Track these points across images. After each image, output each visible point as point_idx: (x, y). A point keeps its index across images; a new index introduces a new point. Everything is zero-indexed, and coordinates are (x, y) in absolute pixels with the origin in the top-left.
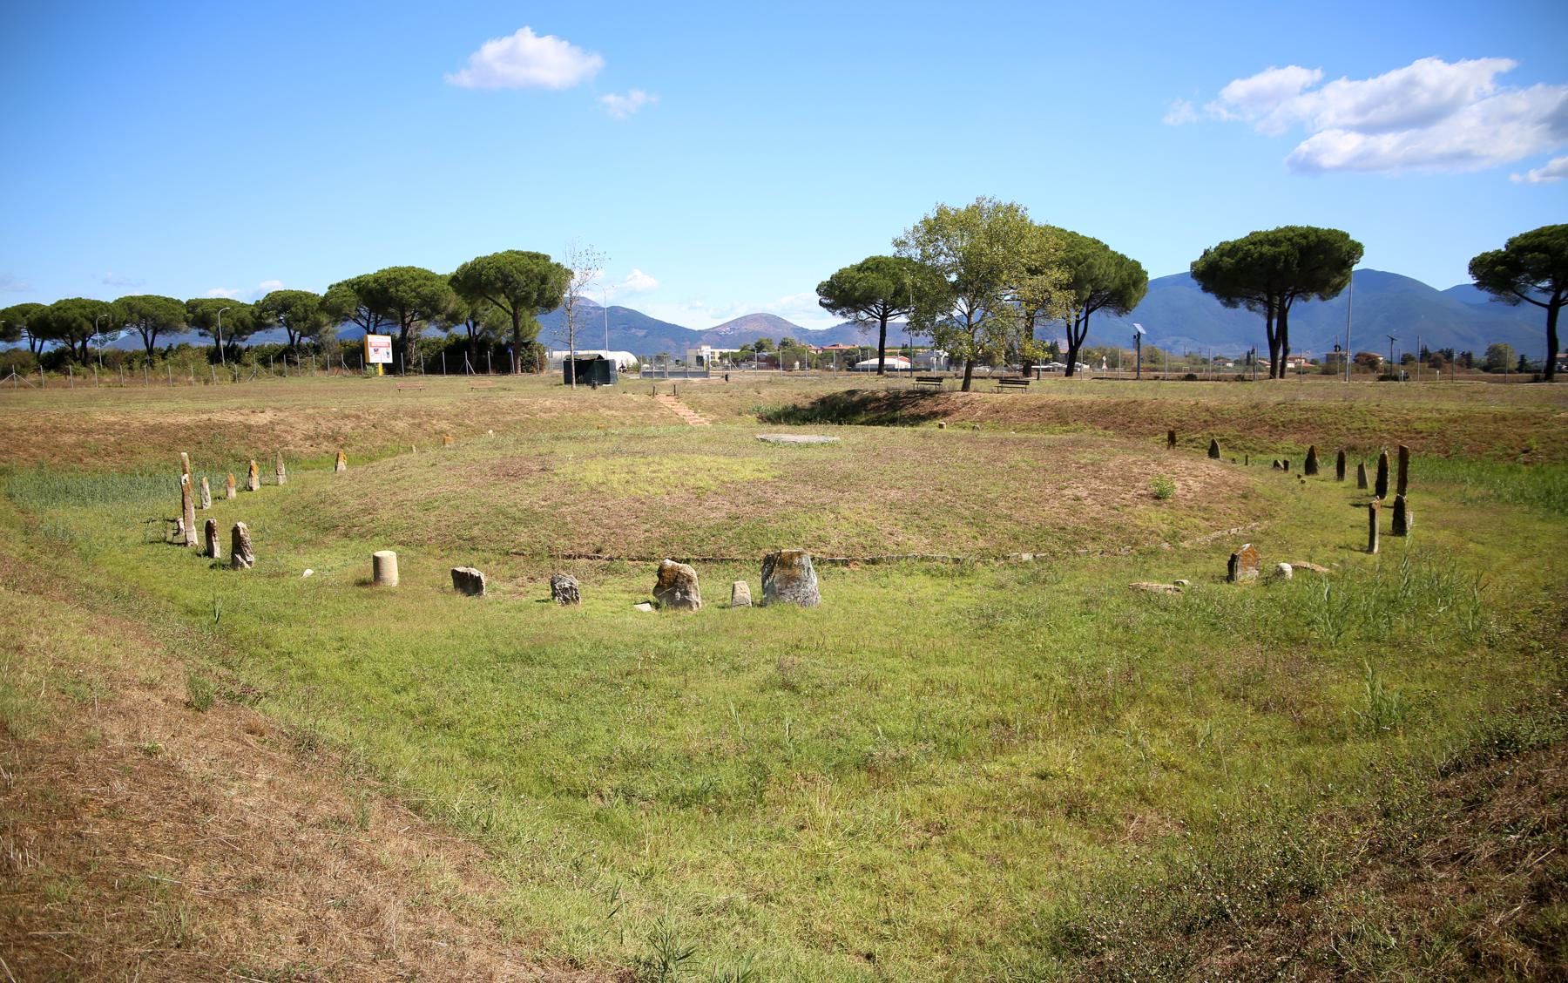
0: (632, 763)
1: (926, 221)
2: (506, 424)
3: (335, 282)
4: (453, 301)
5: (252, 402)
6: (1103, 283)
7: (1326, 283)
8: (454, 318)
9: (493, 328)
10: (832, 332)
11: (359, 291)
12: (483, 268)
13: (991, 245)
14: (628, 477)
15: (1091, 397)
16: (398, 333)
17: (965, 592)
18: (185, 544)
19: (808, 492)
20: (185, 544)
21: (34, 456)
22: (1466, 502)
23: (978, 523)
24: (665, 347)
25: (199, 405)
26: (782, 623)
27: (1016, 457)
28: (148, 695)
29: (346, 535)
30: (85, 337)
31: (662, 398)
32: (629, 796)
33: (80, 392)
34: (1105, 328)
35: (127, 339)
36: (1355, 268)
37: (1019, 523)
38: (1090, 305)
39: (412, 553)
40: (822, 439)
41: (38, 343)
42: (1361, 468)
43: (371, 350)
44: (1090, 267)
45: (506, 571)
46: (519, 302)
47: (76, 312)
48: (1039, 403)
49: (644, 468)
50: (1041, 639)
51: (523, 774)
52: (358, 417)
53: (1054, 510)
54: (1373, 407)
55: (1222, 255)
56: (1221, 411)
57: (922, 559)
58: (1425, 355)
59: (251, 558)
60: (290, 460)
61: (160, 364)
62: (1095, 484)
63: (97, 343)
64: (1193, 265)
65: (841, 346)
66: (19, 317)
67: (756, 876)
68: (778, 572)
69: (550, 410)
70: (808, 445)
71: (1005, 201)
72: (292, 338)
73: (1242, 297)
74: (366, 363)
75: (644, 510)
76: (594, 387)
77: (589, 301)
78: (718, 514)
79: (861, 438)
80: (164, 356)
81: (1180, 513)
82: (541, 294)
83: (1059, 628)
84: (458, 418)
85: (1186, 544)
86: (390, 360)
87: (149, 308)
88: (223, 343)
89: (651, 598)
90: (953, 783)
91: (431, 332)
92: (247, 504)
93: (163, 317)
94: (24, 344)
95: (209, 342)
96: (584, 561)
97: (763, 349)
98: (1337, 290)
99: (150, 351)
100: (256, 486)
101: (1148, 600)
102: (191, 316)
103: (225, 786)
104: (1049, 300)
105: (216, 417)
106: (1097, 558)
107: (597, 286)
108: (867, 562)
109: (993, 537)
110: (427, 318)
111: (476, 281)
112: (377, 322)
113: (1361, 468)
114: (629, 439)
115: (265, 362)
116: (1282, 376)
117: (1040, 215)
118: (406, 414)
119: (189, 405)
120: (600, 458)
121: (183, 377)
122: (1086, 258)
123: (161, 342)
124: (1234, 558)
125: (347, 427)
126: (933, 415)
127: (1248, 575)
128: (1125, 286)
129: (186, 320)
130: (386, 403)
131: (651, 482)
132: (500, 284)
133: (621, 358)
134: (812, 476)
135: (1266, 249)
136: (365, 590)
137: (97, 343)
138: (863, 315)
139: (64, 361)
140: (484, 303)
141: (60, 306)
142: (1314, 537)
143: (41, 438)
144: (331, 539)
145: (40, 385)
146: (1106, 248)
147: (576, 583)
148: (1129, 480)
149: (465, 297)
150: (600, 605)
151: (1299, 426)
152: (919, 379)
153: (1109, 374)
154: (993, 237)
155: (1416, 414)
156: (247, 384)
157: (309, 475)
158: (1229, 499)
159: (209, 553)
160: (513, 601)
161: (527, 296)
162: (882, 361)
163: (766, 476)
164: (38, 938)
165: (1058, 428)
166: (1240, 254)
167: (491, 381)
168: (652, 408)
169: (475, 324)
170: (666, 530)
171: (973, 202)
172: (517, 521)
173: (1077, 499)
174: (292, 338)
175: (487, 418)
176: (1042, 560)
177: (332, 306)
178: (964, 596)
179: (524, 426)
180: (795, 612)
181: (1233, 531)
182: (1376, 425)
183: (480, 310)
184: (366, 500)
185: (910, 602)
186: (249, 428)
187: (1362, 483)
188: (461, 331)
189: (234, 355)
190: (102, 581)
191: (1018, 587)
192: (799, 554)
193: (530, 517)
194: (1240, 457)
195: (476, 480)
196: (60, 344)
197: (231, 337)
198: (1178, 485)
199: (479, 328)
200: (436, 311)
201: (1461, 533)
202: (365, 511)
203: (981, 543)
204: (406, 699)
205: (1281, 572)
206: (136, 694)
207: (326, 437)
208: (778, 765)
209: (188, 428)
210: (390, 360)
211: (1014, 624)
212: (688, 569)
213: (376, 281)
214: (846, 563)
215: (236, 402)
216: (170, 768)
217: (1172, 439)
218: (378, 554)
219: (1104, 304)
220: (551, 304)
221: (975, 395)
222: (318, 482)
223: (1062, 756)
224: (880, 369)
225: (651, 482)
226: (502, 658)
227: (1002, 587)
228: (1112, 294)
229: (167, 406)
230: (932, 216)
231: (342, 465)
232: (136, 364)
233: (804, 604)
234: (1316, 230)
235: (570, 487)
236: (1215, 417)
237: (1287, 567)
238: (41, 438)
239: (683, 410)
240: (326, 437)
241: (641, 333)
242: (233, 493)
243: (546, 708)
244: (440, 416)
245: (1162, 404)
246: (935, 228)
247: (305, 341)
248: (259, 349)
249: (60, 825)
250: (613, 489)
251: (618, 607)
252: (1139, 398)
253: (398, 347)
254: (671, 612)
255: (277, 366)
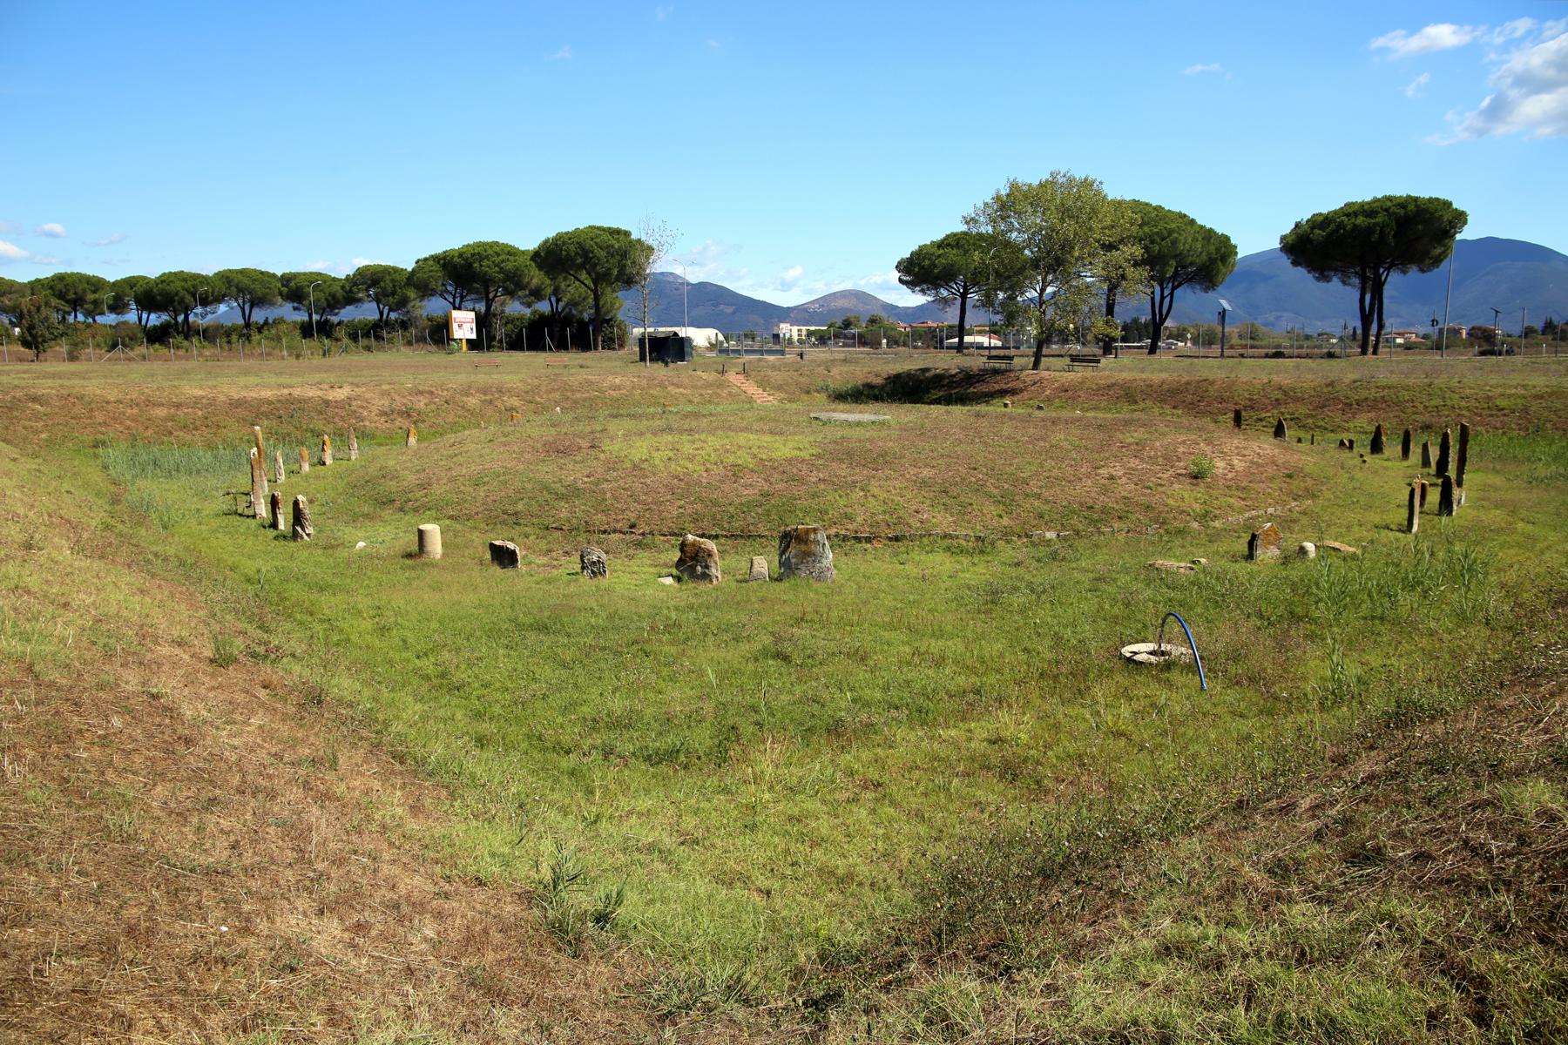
0: (620, 724)
1: (998, 198)
2: (575, 402)
3: (422, 256)
4: (536, 277)
5: (332, 378)
6: (1181, 258)
7: (1426, 254)
8: (537, 294)
9: (576, 304)
10: (921, 308)
11: (444, 266)
12: (564, 243)
13: (1062, 220)
14: (671, 454)
15: (1164, 375)
16: (483, 309)
17: (981, 569)
18: (254, 516)
19: (843, 470)
20: (254, 516)
21: (128, 428)
22: (1533, 481)
23: (1006, 502)
24: (748, 322)
25: (281, 380)
26: (799, 595)
27: (1059, 437)
28: (178, 651)
29: (401, 510)
30: (187, 310)
31: (733, 377)
32: (607, 753)
33: (176, 366)
34: (1190, 305)
35: (225, 312)
36: (1458, 237)
37: (1047, 502)
38: (1178, 280)
39: (459, 527)
40: (873, 418)
41: (145, 316)
42: (1425, 447)
43: (455, 326)
44: (1174, 242)
45: (543, 545)
46: (600, 279)
47: (179, 285)
48: (1109, 382)
49: (687, 445)
50: (1043, 615)
51: (516, 732)
52: (432, 393)
53: (1086, 489)
54: (1454, 383)
55: (1313, 228)
56: (1294, 389)
57: (945, 536)
58: (1549, 327)
59: (310, 530)
60: (363, 435)
61: (256, 337)
62: (1134, 463)
63: (199, 317)
64: (1283, 238)
65: (930, 323)
66: (128, 290)
67: (689, 822)
68: (795, 548)
69: (619, 388)
70: (859, 424)
71: (1079, 175)
72: (381, 313)
73: (1336, 270)
74: (450, 339)
75: (681, 486)
76: (666, 364)
77: (676, 276)
78: (750, 491)
79: (912, 418)
80: (260, 330)
81: (1215, 493)
82: (622, 268)
83: (1061, 604)
84: (528, 396)
85: (1217, 524)
86: (474, 336)
87: (246, 281)
88: (315, 317)
89: (674, 572)
90: (908, 741)
91: (515, 308)
92: (317, 477)
93: (260, 291)
94: (131, 316)
95: (302, 317)
96: (616, 536)
97: (847, 325)
98: (1437, 261)
99: (248, 325)
100: (329, 461)
101: (1153, 575)
102: (285, 290)
103: (217, 728)
104: (1123, 277)
105: (297, 392)
106: (1121, 537)
107: (681, 257)
108: (890, 539)
109: (1019, 515)
110: (511, 294)
111: (559, 257)
112: (462, 298)
113: (1425, 447)
114: (686, 416)
115: (354, 337)
116: (1375, 353)
117: (1118, 188)
118: (478, 390)
119: (273, 380)
120: (649, 436)
121: (277, 352)
122: (1170, 232)
123: (258, 316)
124: (1254, 537)
125: (421, 403)
126: (1003, 393)
127: (1268, 554)
128: (1212, 261)
129: (281, 294)
130: (459, 380)
131: (691, 459)
132: (579, 261)
133: (701, 337)
134: (850, 454)
135: (1360, 220)
136: (408, 562)
137: (199, 317)
138: (944, 293)
139: (168, 335)
140: (565, 279)
141: (165, 279)
142: (1353, 516)
143: (135, 411)
144: (387, 513)
145: (144, 358)
146: (1193, 222)
147: (604, 557)
148: (1169, 459)
149: (547, 273)
150: (625, 578)
151: (1373, 405)
152: (990, 358)
153: (1195, 350)
154: (1066, 212)
155: (1500, 390)
156: (337, 360)
157: (380, 451)
158: (1272, 479)
159: (274, 525)
160: (544, 573)
161: (607, 274)
162: (961, 339)
163: (805, 454)
164: (8, 827)
165: (1126, 407)
166: (1333, 226)
167: (571, 358)
168: (720, 386)
169: (558, 300)
170: (699, 507)
171: (1045, 176)
172: (560, 497)
173: (1112, 478)
174: (381, 313)
175: (557, 395)
176: (1065, 539)
177: (419, 281)
178: (977, 572)
179: (588, 404)
180: (808, 585)
181: (1271, 510)
182: (1455, 403)
183: (563, 286)
184: (422, 475)
185: (923, 578)
186: (327, 403)
187: (1426, 462)
188: (544, 307)
189: (325, 329)
190: (171, 551)
191: (1035, 564)
192: (815, 530)
193: (573, 492)
194: (1306, 436)
195: (527, 456)
196: (165, 317)
197: (327, 312)
198: (1221, 464)
199: (561, 304)
200: (520, 286)
201: (1513, 512)
202: (422, 487)
203: (1005, 521)
204: (427, 664)
205: (1303, 551)
206: (164, 650)
207: (401, 413)
208: (751, 729)
209: (270, 403)
210: (474, 336)
211: (1018, 600)
212: (711, 545)
213: (460, 255)
214: (868, 540)
215: (318, 377)
216: (171, 711)
217: (1238, 420)
218: (422, 527)
219: (1189, 280)
220: (628, 281)
221: (1045, 374)
222: (390, 458)
223: (1017, 726)
224: (960, 347)
225: (691, 459)
226: (520, 627)
227: (1018, 564)
228: (1199, 270)
229: (252, 380)
230: (1004, 192)
231: (412, 440)
232: (234, 338)
233: (818, 579)
234: (1416, 199)
235: (613, 465)
236: (1288, 395)
237: (1310, 546)
238: (135, 411)
239: (752, 389)
240: (401, 413)
241: (729, 310)
242: (306, 467)
243: (547, 672)
244: (511, 392)
245: (1234, 382)
246: (1006, 206)
247: (393, 316)
248: (351, 324)
249: (55, 747)
250: (654, 466)
251: (643, 579)
252: (1211, 377)
253: (482, 322)
254: (692, 585)
255: (366, 342)
